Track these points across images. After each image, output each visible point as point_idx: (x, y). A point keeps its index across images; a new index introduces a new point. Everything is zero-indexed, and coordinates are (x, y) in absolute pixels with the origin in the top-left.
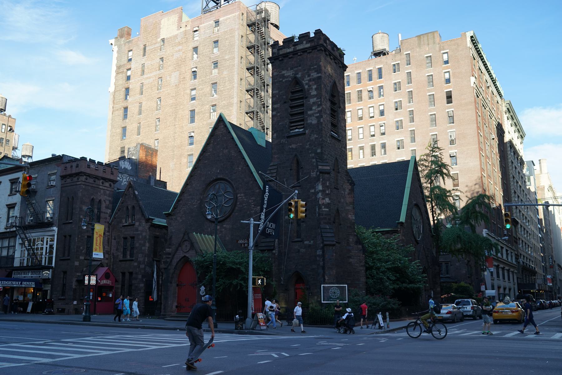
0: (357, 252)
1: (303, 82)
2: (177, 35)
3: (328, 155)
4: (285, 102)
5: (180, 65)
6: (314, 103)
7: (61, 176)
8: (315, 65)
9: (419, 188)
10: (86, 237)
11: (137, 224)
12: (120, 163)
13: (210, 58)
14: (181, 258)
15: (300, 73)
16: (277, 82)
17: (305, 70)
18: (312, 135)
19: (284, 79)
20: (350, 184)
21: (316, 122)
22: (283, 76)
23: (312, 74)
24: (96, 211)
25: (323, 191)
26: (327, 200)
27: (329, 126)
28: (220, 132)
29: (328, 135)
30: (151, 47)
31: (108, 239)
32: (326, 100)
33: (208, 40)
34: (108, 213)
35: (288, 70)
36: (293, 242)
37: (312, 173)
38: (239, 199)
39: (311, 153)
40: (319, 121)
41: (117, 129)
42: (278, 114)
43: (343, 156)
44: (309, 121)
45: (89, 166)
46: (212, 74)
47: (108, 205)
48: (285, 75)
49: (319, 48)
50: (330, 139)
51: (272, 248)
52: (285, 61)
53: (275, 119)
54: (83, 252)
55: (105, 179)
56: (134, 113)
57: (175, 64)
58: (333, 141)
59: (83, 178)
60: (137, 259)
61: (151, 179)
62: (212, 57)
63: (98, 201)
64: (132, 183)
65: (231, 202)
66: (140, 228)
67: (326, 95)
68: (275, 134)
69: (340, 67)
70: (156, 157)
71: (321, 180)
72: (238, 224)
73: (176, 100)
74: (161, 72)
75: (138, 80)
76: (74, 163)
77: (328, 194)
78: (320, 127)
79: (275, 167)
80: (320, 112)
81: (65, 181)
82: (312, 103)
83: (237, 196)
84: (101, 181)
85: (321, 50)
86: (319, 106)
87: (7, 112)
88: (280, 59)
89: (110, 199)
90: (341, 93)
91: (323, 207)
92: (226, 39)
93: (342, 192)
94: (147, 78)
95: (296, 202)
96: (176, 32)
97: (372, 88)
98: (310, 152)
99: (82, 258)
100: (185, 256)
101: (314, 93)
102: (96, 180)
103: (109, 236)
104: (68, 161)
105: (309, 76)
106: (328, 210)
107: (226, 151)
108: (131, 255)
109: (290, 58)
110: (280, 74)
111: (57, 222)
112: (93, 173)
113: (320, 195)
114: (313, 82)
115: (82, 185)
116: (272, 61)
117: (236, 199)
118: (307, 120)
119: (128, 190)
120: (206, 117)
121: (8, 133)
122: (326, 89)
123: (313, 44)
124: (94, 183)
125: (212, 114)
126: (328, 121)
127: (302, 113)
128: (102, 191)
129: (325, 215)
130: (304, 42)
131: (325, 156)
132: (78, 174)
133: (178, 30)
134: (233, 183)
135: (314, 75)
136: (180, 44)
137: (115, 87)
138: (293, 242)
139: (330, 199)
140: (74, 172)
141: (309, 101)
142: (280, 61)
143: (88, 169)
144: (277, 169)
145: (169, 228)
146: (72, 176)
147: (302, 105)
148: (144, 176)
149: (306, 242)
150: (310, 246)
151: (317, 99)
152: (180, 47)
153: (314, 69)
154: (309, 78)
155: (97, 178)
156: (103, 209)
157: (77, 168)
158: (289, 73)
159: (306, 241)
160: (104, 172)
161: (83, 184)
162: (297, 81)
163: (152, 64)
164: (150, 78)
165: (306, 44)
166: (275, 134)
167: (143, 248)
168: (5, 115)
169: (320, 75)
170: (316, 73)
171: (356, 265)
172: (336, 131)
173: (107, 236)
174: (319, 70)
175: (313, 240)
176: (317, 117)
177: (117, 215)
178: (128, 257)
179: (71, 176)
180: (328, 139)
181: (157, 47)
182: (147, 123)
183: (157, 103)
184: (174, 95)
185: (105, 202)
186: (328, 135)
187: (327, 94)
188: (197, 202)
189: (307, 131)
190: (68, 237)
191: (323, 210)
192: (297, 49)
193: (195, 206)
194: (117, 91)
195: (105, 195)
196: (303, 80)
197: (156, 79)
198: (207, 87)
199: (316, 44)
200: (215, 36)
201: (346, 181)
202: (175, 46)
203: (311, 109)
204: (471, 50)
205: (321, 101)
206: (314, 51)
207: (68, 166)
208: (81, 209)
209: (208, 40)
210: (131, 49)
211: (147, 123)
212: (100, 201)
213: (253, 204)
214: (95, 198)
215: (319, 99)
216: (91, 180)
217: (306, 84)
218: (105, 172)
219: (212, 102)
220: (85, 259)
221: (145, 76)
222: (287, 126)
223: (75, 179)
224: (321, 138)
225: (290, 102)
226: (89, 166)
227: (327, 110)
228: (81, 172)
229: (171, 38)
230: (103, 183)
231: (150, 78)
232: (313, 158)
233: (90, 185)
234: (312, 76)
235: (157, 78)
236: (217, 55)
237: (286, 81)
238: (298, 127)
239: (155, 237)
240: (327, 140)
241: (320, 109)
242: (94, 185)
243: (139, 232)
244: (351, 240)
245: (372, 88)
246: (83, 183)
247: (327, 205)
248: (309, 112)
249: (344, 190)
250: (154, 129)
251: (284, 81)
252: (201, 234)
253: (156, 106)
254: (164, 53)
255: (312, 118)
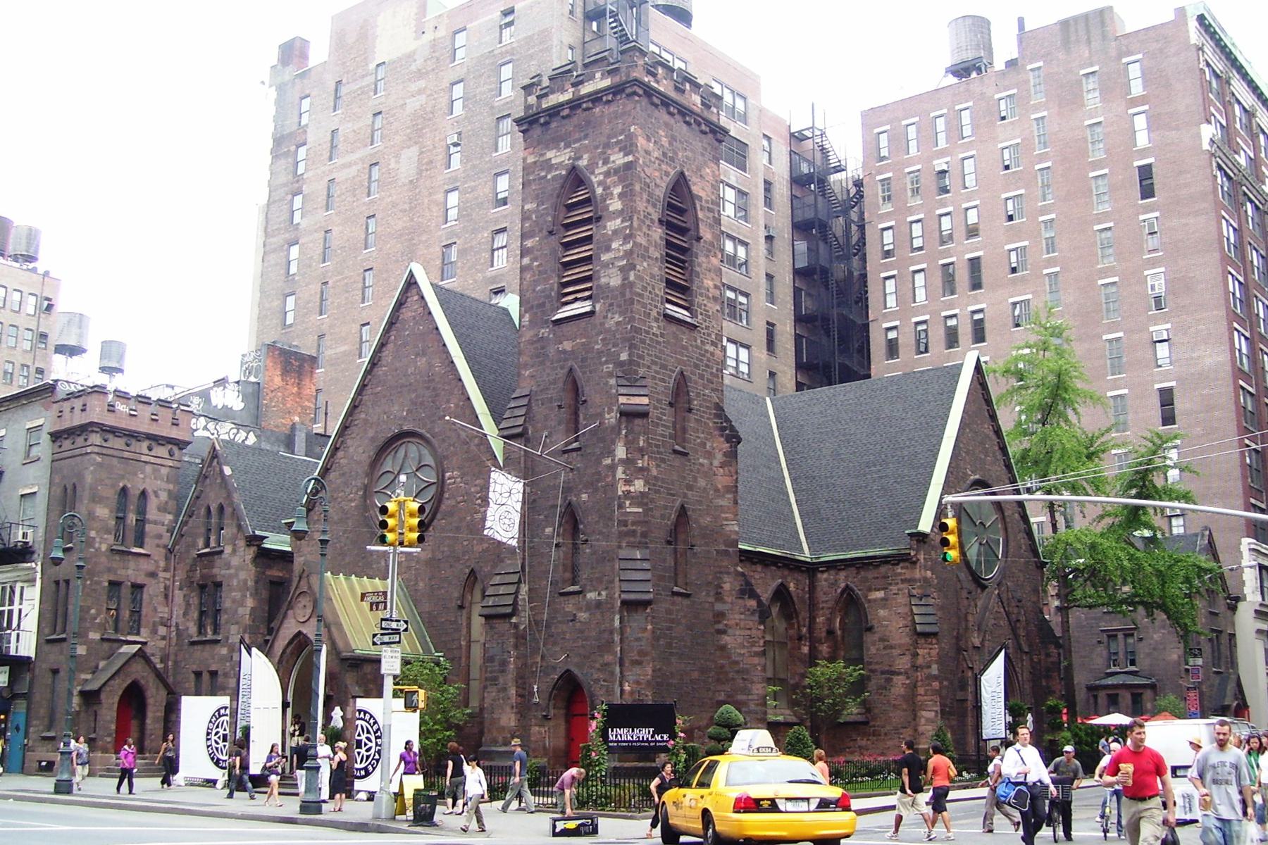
0: (742, 616)
1: (593, 177)
2: (414, 52)
3: (654, 367)
4: (551, 233)
5: (422, 129)
6: (615, 232)
7: (51, 434)
8: (621, 134)
9: (994, 437)
10: (106, 584)
11: (228, 549)
12: (212, 393)
13: (492, 107)
14: (291, 636)
15: (586, 156)
16: (534, 180)
17: (597, 147)
18: (609, 315)
19: (549, 172)
20: (728, 440)
21: (619, 282)
22: (548, 166)
23: (612, 158)
24: (132, 518)
25: (628, 462)
26: (639, 485)
27: (660, 289)
28: (410, 314)
29: (654, 313)
30: (354, 87)
31: (166, 588)
32: (648, 222)
33: (487, 61)
34: (166, 523)
35: (559, 149)
36: (562, 594)
37: (607, 416)
38: (450, 484)
39: (606, 362)
40: (625, 278)
41: (272, 301)
42: (535, 264)
43: (707, 366)
44: (603, 280)
45: (111, 408)
46: (496, 150)
47: (166, 502)
48: (553, 162)
49: (629, 90)
50: (661, 324)
51: (509, 610)
52: (553, 125)
53: (528, 276)
54: (97, 621)
55: (155, 439)
56: (312, 257)
57: (408, 128)
58: (673, 328)
59: (96, 439)
60: (227, 638)
61: (297, 433)
62: (497, 104)
63: (138, 492)
64: (218, 448)
65: (432, 490)
66: (235, 561)
67: (650, 209)
68: (527, 315)
69: (704, 133)
70: (311, 376)
71: (624, 432)
72: (446, 549)
73: (412, 220)
74: (376, 150)
75: (324, 172)
76: (76, 400)
77: (642, 469)
78: (628, 295)
79: (524, 401)
80: (629, 254)
81: (60, 446)
82: (610, 233)
83: (443, 476)
84: (145, 444)
85: (635, 93)
86: (627, 239)
87: (41, 266)
88: (542, 120)
89: (171, 487)
90: (707, 202)
91: (628, 503)
92: (531, 56)
93: (701, 460)
94: (344, 166)
95: (401, 505)
96: (411, 45)
97: (947, 163)
98: (604, 359)
99: (94, 636)
100: (300, 633)
101: (615, 205)
102: (133, 441)
103: (169, 579)
104: (65, 397)
105: (606, 162)
106: (641, 510)
107: (422, 362)
108: (215, 632)
109: (563, 117)
110: (541, 159)
111: (42, 546)
112: (123, 425)
113: (620, 473)
114: (616, 178)
115: (93, 456)
116: (524, 128)
117: (441, 483)
118: (599, 278)
119: (210, 465)
120: (482, 261)
121: (43, 315)
122: (650, 195)
123: (617, 79)
124: (128, 448)
125: (496, 253)
126: (653, 276)
127: (588, 260)
128: (148, 468)
129: (634, 523)
130: (598, 75)
131: (642, 371)
132: (84, 429)
133: (417, 38)
134: (434, 441)
135: (618, 159)
136: (420, 74)
137: (270, 191)
138: (562, 594)
139: (647, 482)
140: (76, 423)
141: (605, 227)
142: (542, 125)
143: (110, 414)
144: (528, 406)
145: (298, 561)
146: (73, 433)
147: (588, 239)
148: (277, 426)
149: (591, 596)
150: (599, 604)
151: (622, 222)
152: (422, 83)
153: (618, 142)
154: (605, 169)
155: (132, 435)
156: (152, 513)
157: (84, 413)
158: (560, 157)
159: (590, 591)
160: (153, 420)
161: (98, 453)
162: (576, 179)
163: (355, 128)
164: (348, 167)
165: (602, 79)
166: (527, 315)
167: (241, 611)
168: (34, 270)
169: (630, 158)
170: (622, 154)
171: (738, 651)
172: (685, 300)
173: (162, 580)
174: (628, 147)
175: (606, 589)
176: (622, 269)
177: (185, 528)
178: (210, 636)
179: (71, 433)
180: (654, 324)
181: (368, 85)
182: (342, 283)
183: (367, 228)
184: (407, 206)
185: (157, 496)
186: (654, 313)
187: (654, 206)
188: (356, 493)
189: (598, 307)
190: (62, 585)
191: (628, 510)
192: (582, 93)
193: (353, 504)
194: (275, 202)
195: (155, 479)
196: (593, 173)
197: (364, 168)
198: (486, 183)
199: (624, 78)
200: (503, 49)
201: (717, 433)
202: (410, 80)
203: (608, 249)
204: (1200, 52)
205: (631, 226)
206: (618, 97)
207: (66, 406)
208: (91, 515)
209: (487, 61)
210: (307, 92)
211: (342, 283)
212: (143, 494)
213: (480, 498)
214: (129, 486)
215: (626, 221)
216: (118, 443)
217: (600, 183)
218: (156, 420)
219: (496, 221)
220: (102, 639)
221: (338, 161)
222: (553, 294)
223: (80, 441)
224: (629, 322)
225: (562, 232)
226: (111, 408)
227: (652, 249)
228: (92, 424)
229: (400, 59)
230: (150, 449)
231: (350, 165)
232: (610, 375)
233: (116, 453)
234: (614, 162)
235: (367, 166)
236: (508, 100)
237: (553, 178)
238: (579, 295)
239: (272, 583)
240: (650, 327)
241: (629, 246)
242: (126, 455)
243: (232, 571)
244: (727, 586)
245: (947, 163)
246: (96, 449)
247: (640, 499)
248: (605, 257)
249: (710, 455)
250: (359, 298)
251: (549, 177)
252: (347, 575)
253: (363, 237)
254: (383, 100)
255: (611, 271)
